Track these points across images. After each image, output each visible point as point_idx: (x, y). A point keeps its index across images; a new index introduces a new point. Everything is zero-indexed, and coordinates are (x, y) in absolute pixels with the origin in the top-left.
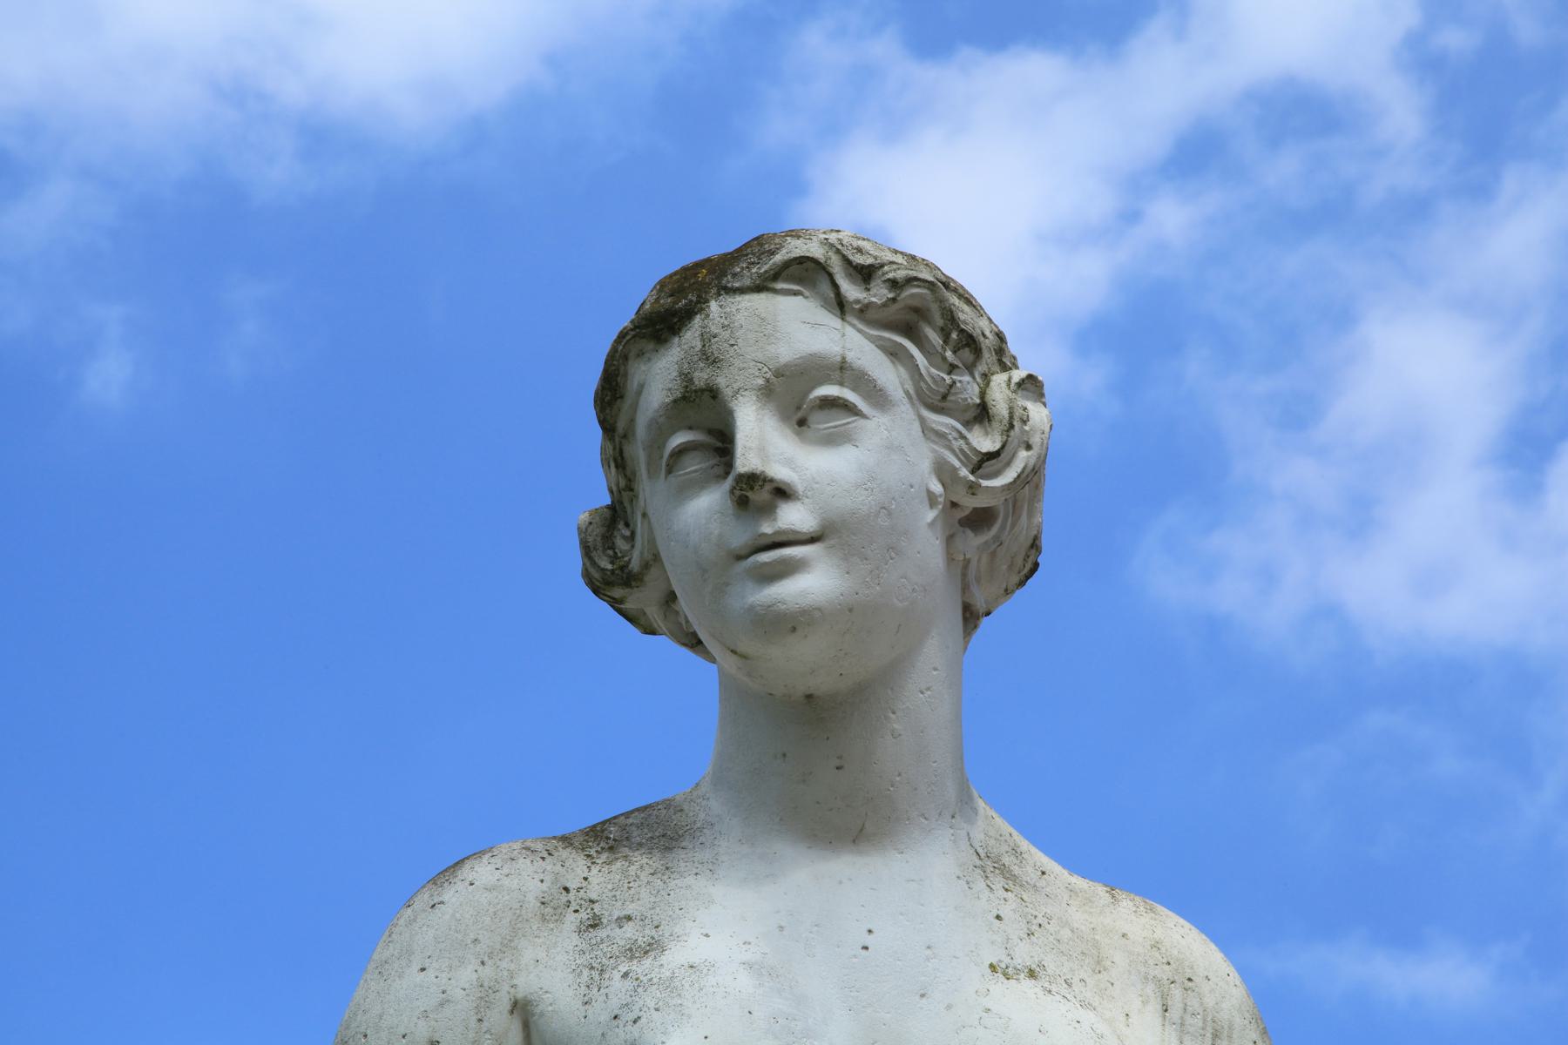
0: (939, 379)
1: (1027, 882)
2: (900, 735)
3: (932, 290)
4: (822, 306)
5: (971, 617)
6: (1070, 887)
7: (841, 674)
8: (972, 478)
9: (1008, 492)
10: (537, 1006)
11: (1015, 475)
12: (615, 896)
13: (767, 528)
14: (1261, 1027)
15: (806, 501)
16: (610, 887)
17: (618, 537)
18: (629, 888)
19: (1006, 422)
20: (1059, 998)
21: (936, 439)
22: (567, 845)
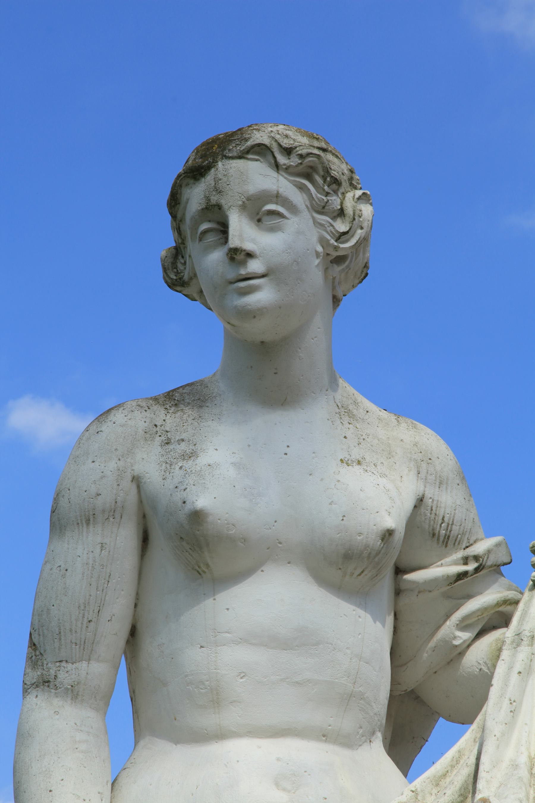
0: (321, 199)
1: (359, 418)
2: (303, 358)
3: (318, 158)
4: (269, 166)
5: (336, 301)
6: (379, 417)
7: (276, 333)
8: (336, 244)
9: (352, 249)
10: (143, 479)
11: (355, 241)
12: (177, 429)
13: (243, 272)
14: (462, 477)
15: (261, 258)
16: (175, 425)
17: (179, 263)
18: (183, 426)
19: (351, 217)
20: (370, 473)
21: (320, 227)
22: (157, 403)
